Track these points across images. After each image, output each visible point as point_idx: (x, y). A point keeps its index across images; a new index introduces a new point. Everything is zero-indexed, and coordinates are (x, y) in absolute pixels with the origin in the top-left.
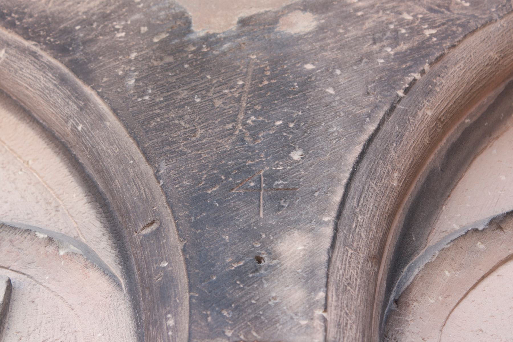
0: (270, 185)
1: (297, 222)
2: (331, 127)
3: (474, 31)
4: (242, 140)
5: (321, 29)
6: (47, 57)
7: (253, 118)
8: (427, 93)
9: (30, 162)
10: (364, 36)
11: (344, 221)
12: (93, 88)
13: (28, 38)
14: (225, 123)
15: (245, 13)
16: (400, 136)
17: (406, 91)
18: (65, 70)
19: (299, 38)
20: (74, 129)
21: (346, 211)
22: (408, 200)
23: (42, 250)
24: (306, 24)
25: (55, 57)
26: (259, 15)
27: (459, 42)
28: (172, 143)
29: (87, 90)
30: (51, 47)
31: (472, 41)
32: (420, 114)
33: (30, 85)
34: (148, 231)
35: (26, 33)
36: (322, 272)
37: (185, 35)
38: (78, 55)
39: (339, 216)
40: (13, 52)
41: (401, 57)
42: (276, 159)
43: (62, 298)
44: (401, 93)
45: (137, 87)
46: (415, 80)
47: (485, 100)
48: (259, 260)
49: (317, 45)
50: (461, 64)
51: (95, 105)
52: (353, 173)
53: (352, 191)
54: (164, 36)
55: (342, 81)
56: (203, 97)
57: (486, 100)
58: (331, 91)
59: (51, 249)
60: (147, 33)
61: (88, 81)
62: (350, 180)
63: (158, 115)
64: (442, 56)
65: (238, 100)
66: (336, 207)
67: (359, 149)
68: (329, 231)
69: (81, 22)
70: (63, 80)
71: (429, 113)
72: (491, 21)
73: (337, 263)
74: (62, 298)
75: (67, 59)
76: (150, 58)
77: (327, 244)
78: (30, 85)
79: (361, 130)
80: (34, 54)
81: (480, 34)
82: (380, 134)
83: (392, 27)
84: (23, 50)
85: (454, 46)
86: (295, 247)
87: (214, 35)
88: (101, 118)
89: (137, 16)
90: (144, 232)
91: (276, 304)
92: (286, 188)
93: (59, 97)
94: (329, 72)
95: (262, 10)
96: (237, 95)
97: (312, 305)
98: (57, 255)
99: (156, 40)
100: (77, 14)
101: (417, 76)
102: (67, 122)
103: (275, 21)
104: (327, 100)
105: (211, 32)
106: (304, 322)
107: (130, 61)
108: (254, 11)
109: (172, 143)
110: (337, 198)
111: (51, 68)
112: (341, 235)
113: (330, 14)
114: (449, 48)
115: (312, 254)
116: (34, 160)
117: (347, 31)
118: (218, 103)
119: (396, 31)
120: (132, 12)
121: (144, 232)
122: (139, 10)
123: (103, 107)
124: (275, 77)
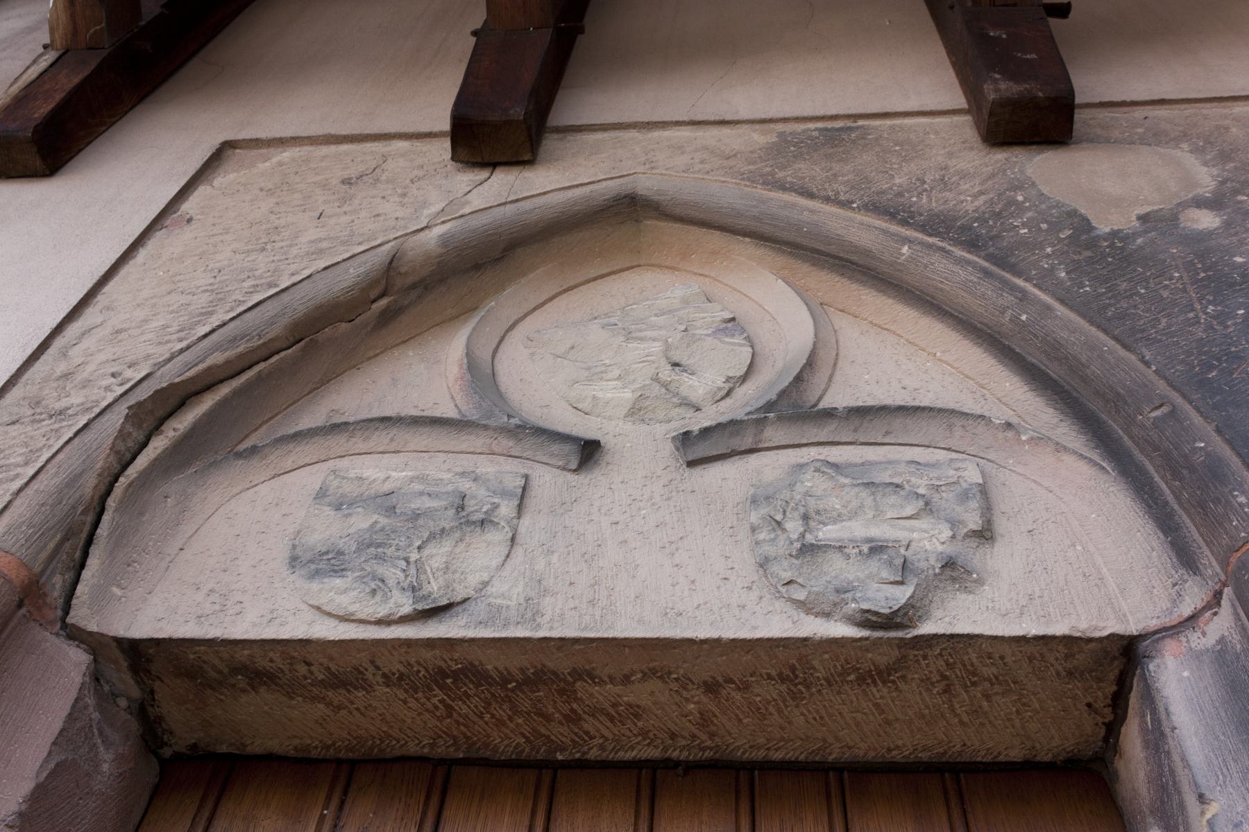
6: (959, 252)
9: (938, 354)
13: (931, 235)
18: (986, 264)
20: (1015, 320)
23: (1000, 435)
25: (969, 252)
29: (1020, 282)
30: (957, 242)
33: (946, 279)
34: (1158, 413)
35: (923, 228)
38: (991, 250)
40: (919, 248)
43: (1035, 481)
51: (1036, 296)
56: (1146, 288)
59: (1010, 434)
61: (1019, 274)
69: (976, 220)
70: (987, 273)
74: (1035, 481)
75: (983, 254)
76: (1067, 252)
78: (946, 279)
80: (943, 249)
84: (930, 246)
87: (1120, 231)
88: (1049, 308)
90: (1153, 414)
93: (987, 289)
95: (1156, 208)
98: (1019, 440)
102: (1003, 313)
105: (1116, 228)
111: (969, 262)
116: (943, 352)
121: (1153, 414)
122: (1028, 209)
124: (1210, 269)
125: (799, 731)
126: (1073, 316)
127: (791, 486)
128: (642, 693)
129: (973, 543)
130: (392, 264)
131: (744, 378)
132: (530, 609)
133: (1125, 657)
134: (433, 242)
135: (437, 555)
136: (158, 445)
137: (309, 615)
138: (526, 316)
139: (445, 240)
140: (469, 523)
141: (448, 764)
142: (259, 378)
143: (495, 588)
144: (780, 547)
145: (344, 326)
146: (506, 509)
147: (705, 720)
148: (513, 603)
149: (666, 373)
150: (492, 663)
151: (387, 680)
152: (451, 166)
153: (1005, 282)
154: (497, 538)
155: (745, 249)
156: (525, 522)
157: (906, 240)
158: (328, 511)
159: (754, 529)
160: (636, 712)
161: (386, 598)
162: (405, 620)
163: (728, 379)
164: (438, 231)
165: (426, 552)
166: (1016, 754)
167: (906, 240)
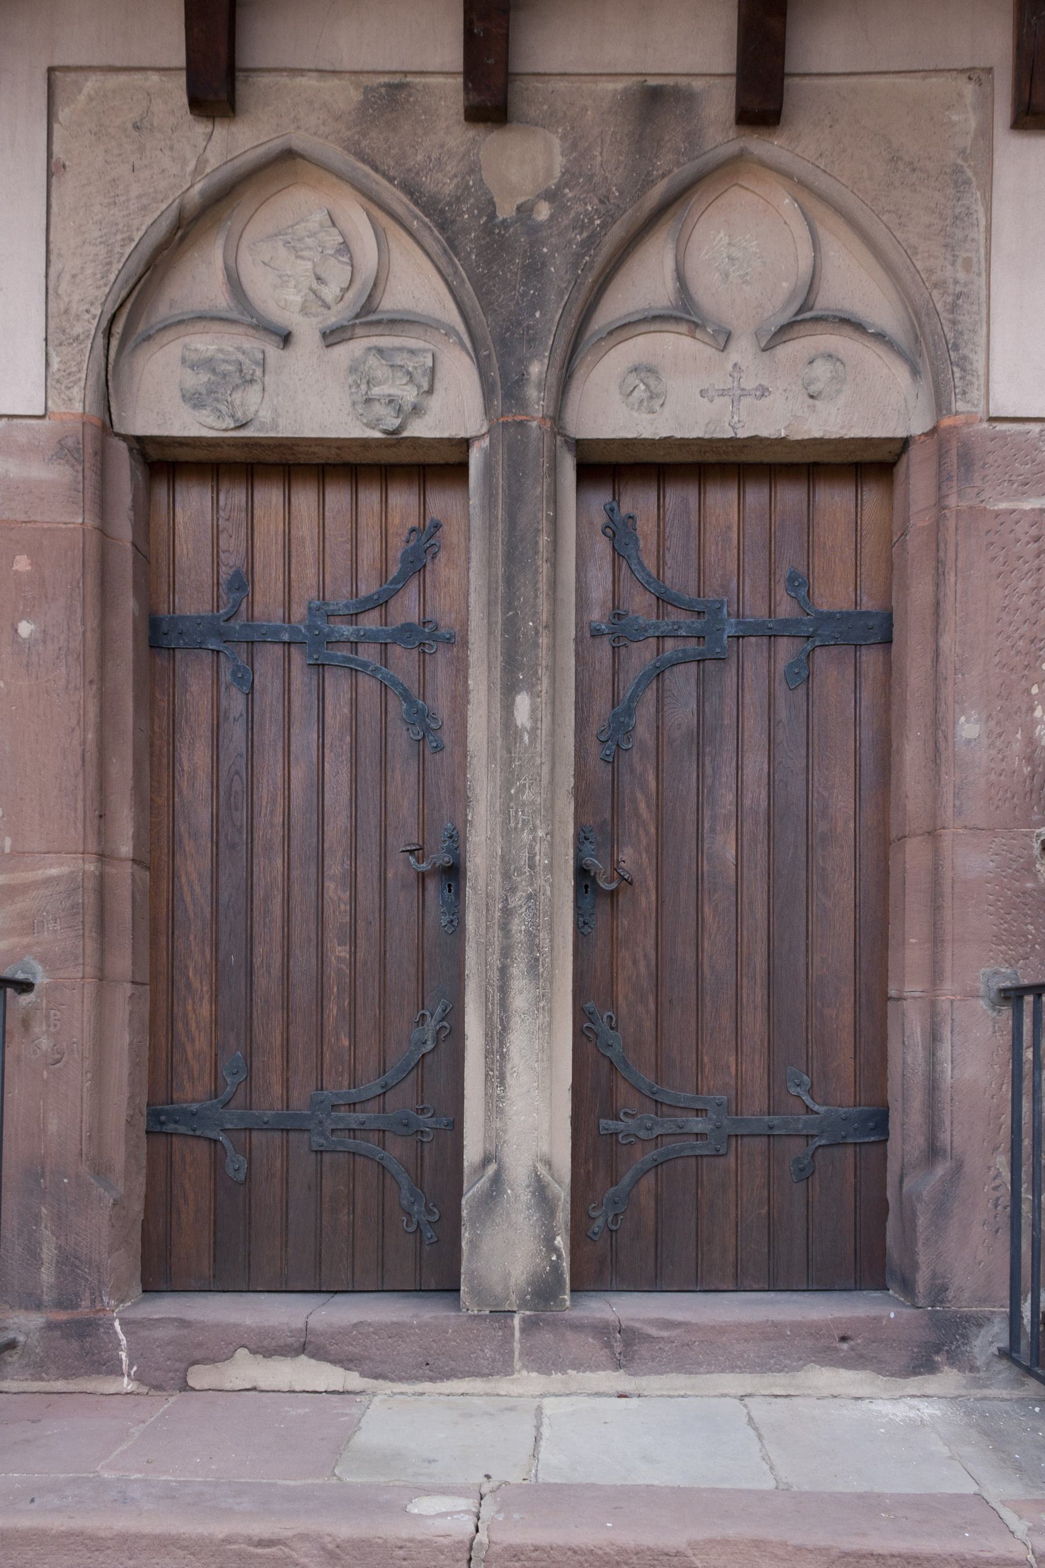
15: (520, 200)
16: (577, 299)
29: (456, 260)
61: (456, 255)
79: (562, 299)
80: (430, 228)
110: (551, 343)
125: (370, 457)
126: (471, 289)
127: (364, 363)
128: (316, 449)
129: (425, 396)
130: (181, 210)
131: (348, 288)
132: (275, 426)
133: (465, 444)
134: (197, 197)
135: (237, 397)
136: (114, 343)
137: (198, 425)
138: (244, 229)
139: (202, 193)
140: (246, 381)
141: (251, 464)
142: (139, 293)
143: (260, 414)
144: (359, 398)
145: (166, 252)
146: (259, 372)
147: (338, 455)
148: (268, 421)
149: (315, 285)
150: (263, 442)
151: (229, 445)
152: (190, 117)
153: (451, 259)
154: (257, 387)
155: (347, 189)
156: (267, 378)
157: (416, 217)
158: (189, 371)
159: (350, 387)
160: (314, 453)
161: (224, 420)
162: (232, 429)
163: (342, 289)
164: (198, 187)
165: (233, 396)
166: (442, 462)
167: (416, 217)
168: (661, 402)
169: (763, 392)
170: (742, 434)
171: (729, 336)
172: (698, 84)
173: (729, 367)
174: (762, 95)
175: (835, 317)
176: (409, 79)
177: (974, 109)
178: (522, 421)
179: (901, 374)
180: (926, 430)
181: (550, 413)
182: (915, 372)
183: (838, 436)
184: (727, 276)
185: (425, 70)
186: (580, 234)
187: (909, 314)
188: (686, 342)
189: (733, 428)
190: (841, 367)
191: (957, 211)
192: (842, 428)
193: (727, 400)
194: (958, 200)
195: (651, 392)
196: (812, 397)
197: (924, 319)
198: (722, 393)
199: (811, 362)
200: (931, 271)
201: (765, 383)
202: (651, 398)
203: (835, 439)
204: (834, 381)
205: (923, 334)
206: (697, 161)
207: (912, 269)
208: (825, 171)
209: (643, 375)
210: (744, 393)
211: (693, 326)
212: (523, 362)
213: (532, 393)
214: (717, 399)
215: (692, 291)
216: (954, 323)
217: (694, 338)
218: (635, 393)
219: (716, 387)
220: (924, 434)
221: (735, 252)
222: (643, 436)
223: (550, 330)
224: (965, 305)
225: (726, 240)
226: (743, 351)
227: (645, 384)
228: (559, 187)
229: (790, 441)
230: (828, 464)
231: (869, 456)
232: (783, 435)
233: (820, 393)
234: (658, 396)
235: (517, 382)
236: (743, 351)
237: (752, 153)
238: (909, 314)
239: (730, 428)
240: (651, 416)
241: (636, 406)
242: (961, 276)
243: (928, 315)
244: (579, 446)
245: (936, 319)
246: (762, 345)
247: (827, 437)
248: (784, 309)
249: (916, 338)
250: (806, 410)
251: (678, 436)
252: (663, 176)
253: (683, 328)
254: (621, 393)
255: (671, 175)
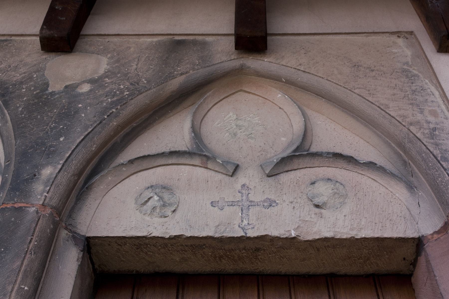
0: (49, 149)
1: (51, 163)
2: (77, 129)
3: (142, 93)
4: (47, 133)
5: (91, 91)
7: (54, 125)
8: (116, 117)
10: (104, 94)
11: (67, 163)
12: (7, 111)
14: (44, 126)
15: (68, 83)
16: (100, 132)
17: (108, 116)
19: (82, 94)
21: (70, 159)
22: (101, 154)
24: (86, 88)
26: (72, 84)
27: (135, 97)
28: (25, 133)
31: (140, 97)
32: (111, 124)
36: (51, 181)
37: (45, 91)
39: (65, 162)
41: (112, 103)
42: (55, 140)
44: (106, 117)
45: (21, 111)
46: (113, 112)
47: (143, 117)
48: (35, 175)
49: (86, 97)
50: (133, 105)
52: (77, 146)
53: (74, 152)
54: (38, 91)
55: (88, 111)
57: (143, 117)
58: (83, 115)
60: (33, 90)
62: (75, 149)
63: (24, 122)
64: (126, 103)
65: (52, 118)
66: (65, 158)
67: (82, 137)
68: (60, 166)
71: (115, 124)
72: (150, 89)
73: (59, 177)
77: (57, 171)
79: (86, 130)
81: (144, 94)
82: (93, 132)
83: (115, 91)
85: (132, 99)
86: (47, 172)
87: (55, 91)
89: (32, 83)
91: (34, 191)
92: (54, 151)
94: (86, 108)
96: (52, 115)
97: (44, 191)
99: (35, 93)
100: (12, 82)
101: (114, 110)
103: (77, 87)
104: (81, 118)
105: (54, 90)
106: (39, 197)
107: (23, 101)
108: (71, 83)
109: (25, 133)
110: (68, 155)
112: (64, 168)
113: (96, 85)
114: (130, 100)
115: (51, 174)
117: (99, 92)
118: (45, 118)
119: (115, 92)
120: (31, 81)
123: (9, 118)
168: (173, 209)
169: (271, 203)
170: (252, 234)
171: (237, 167)
172: (209, 39)
173: (239, 187)
174: (252, 39)
175: (328, 153)
176: (13, 38)
177: (407, 48)
178: (21, 207)
179: (400, 192)
180: (437, 229)
181: (54, 202)
182: (411, 187)
183: (349, 236)
184: (235, 135)
185: (24, 33)
186: (111, 98)
187: (393, 148)
188: (200, 172)
189: (243, 229)
190: (341, 187)
191: (414, 88)
192: (352, 229)
193: (237, 209)
194: (413, 83)
195: (164, 202)
196: (317, 206)
197: (408, 145)
198: (232, 204)
199: (313, 183)
200: (404, 117)
201: (272, 197)
202: (164, 205)
203: (346, 239)
204: (337, 196)
205: (411, 158)
206: (208, 69)
207: (387, 116)
208: (304, 72)
209: (157, 190)
210: (252, 204)
211: (205, 159)
212: (38, 167)
213: (39, 188)
214: (227, 209)
215: (206, 142)
216: (437, 145)
217: (207, 168)
218: (149, 203)
219: (226, 200)
220: (435, 232)
221: (240, 123)
222: (153, 235)
223: (69, 148)
224: (442, 135)
225: (235, 117)
226: (250, 177)
227: (158, 196)
228: (101, 78)
229: (301, 242)
230: (345, 276)
231: (383, 265)
232: (293, 235)
233: (325, 204)
234: (170, 205)
235: (27, 180)
236: (250, 177)
237: (249, 67)
238: (393, 148)
239: (240, 229)
240: (163, 220)
241: (149, 212)
242: (431, 118)
243: (411, 142)
244: (91, 247)
245: (419, 143)
246: (267, 172)
247: (338, 237)
248: (284, 151)
249: (405, 163)
250: (313, 216)
251: (188, 234)
252: (182, 74)
253: (197, 161)
254: (136, 203)
255: (187, 75)
